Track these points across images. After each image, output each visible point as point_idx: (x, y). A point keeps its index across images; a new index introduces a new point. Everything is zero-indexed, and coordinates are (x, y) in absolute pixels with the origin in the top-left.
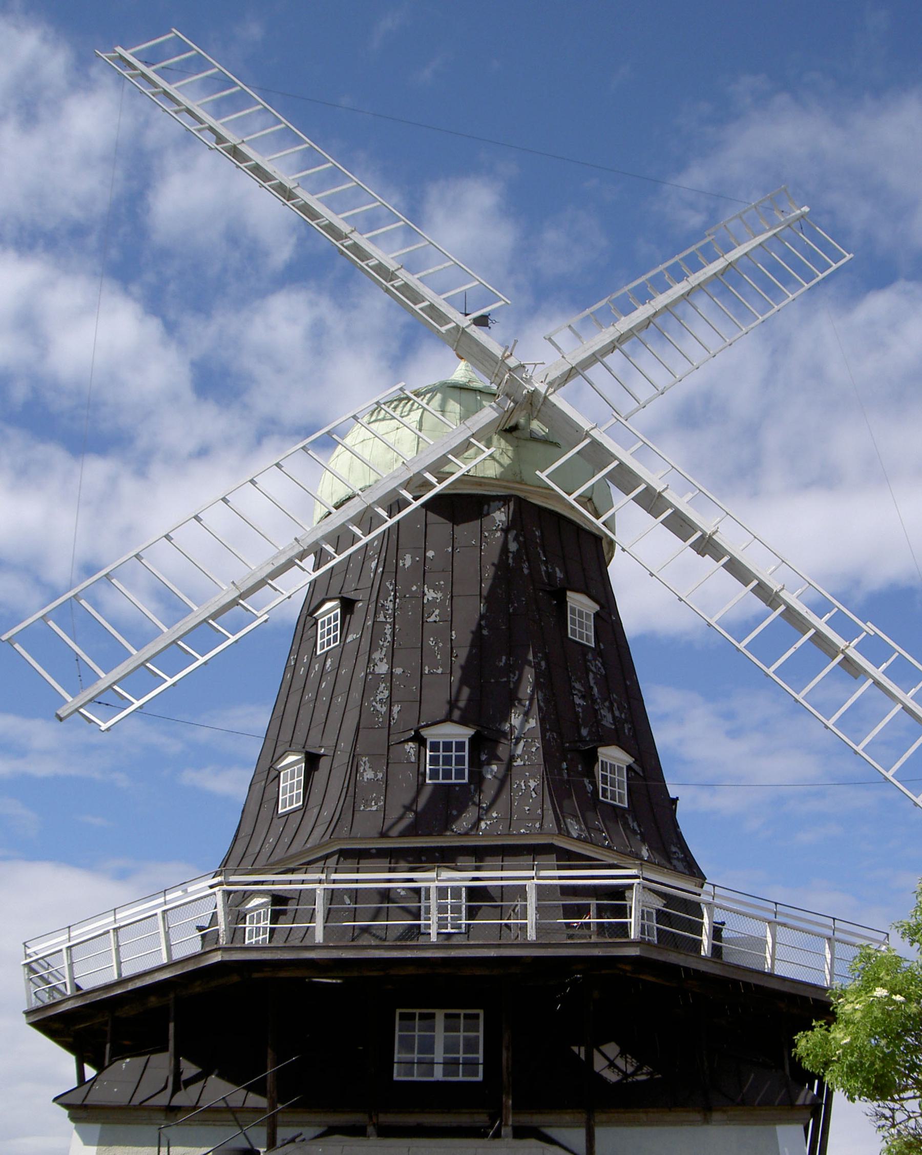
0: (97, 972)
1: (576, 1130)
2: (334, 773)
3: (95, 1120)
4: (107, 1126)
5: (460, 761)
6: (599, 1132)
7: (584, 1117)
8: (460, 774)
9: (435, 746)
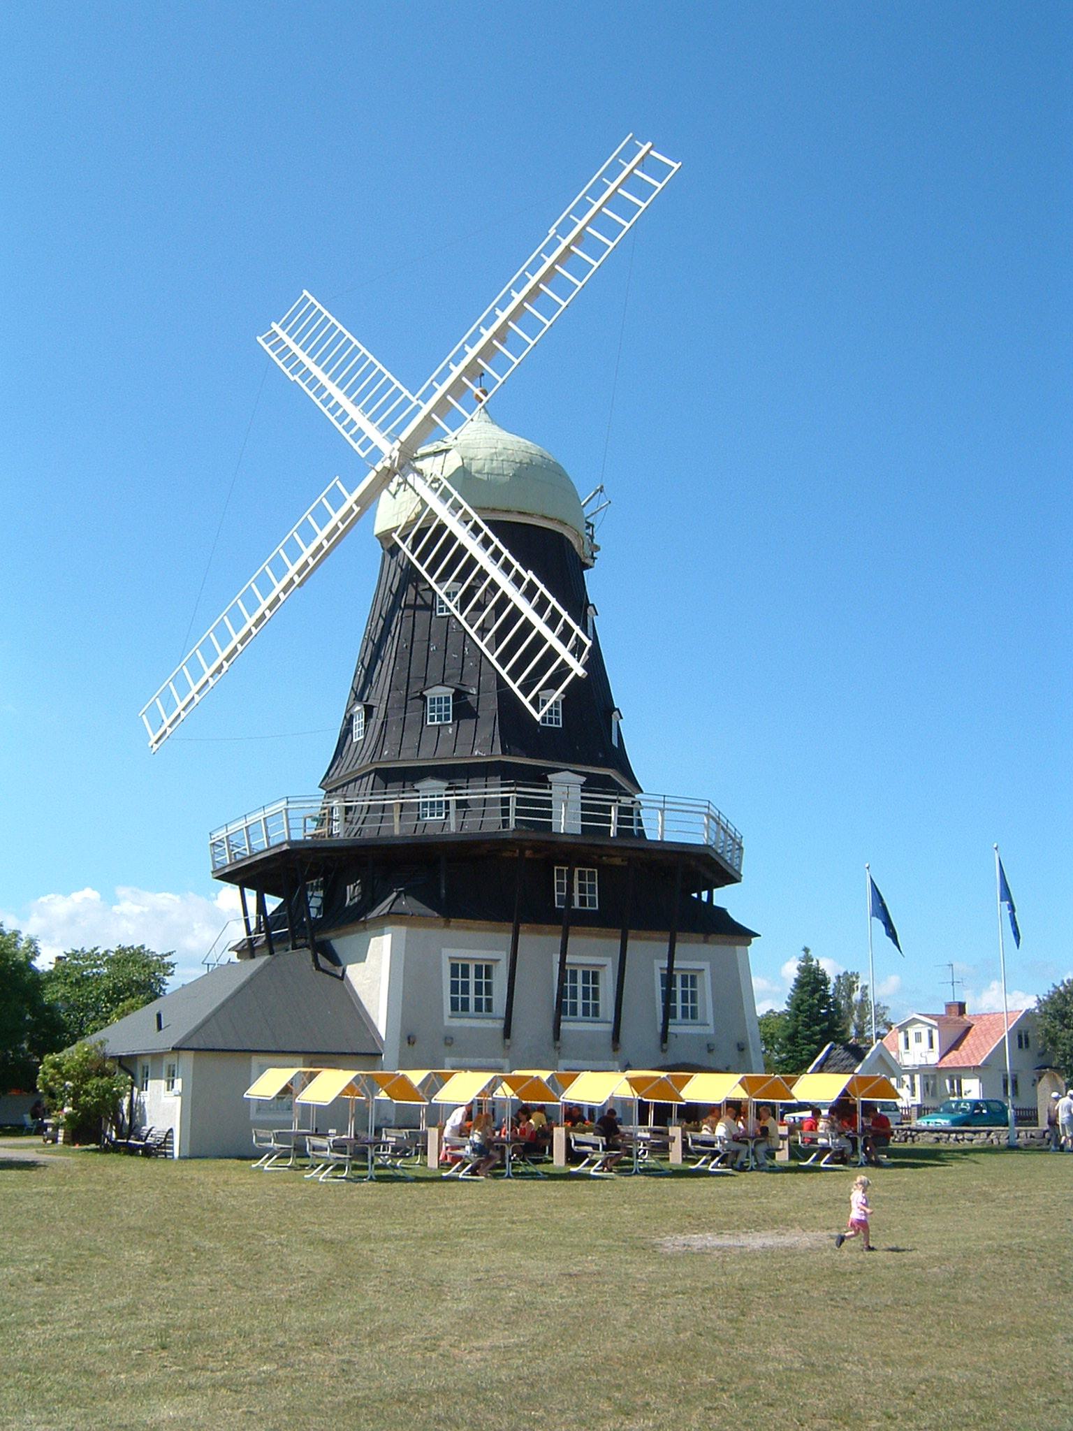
0: (261, 844)
1: (657, 944)
2: (377, 721)
3: (401, 923)
4: (414, 930)
5: (447, 709)
6: (630, 943)
7: (667, 935)
8: (557, 722)
9: (432, 702)
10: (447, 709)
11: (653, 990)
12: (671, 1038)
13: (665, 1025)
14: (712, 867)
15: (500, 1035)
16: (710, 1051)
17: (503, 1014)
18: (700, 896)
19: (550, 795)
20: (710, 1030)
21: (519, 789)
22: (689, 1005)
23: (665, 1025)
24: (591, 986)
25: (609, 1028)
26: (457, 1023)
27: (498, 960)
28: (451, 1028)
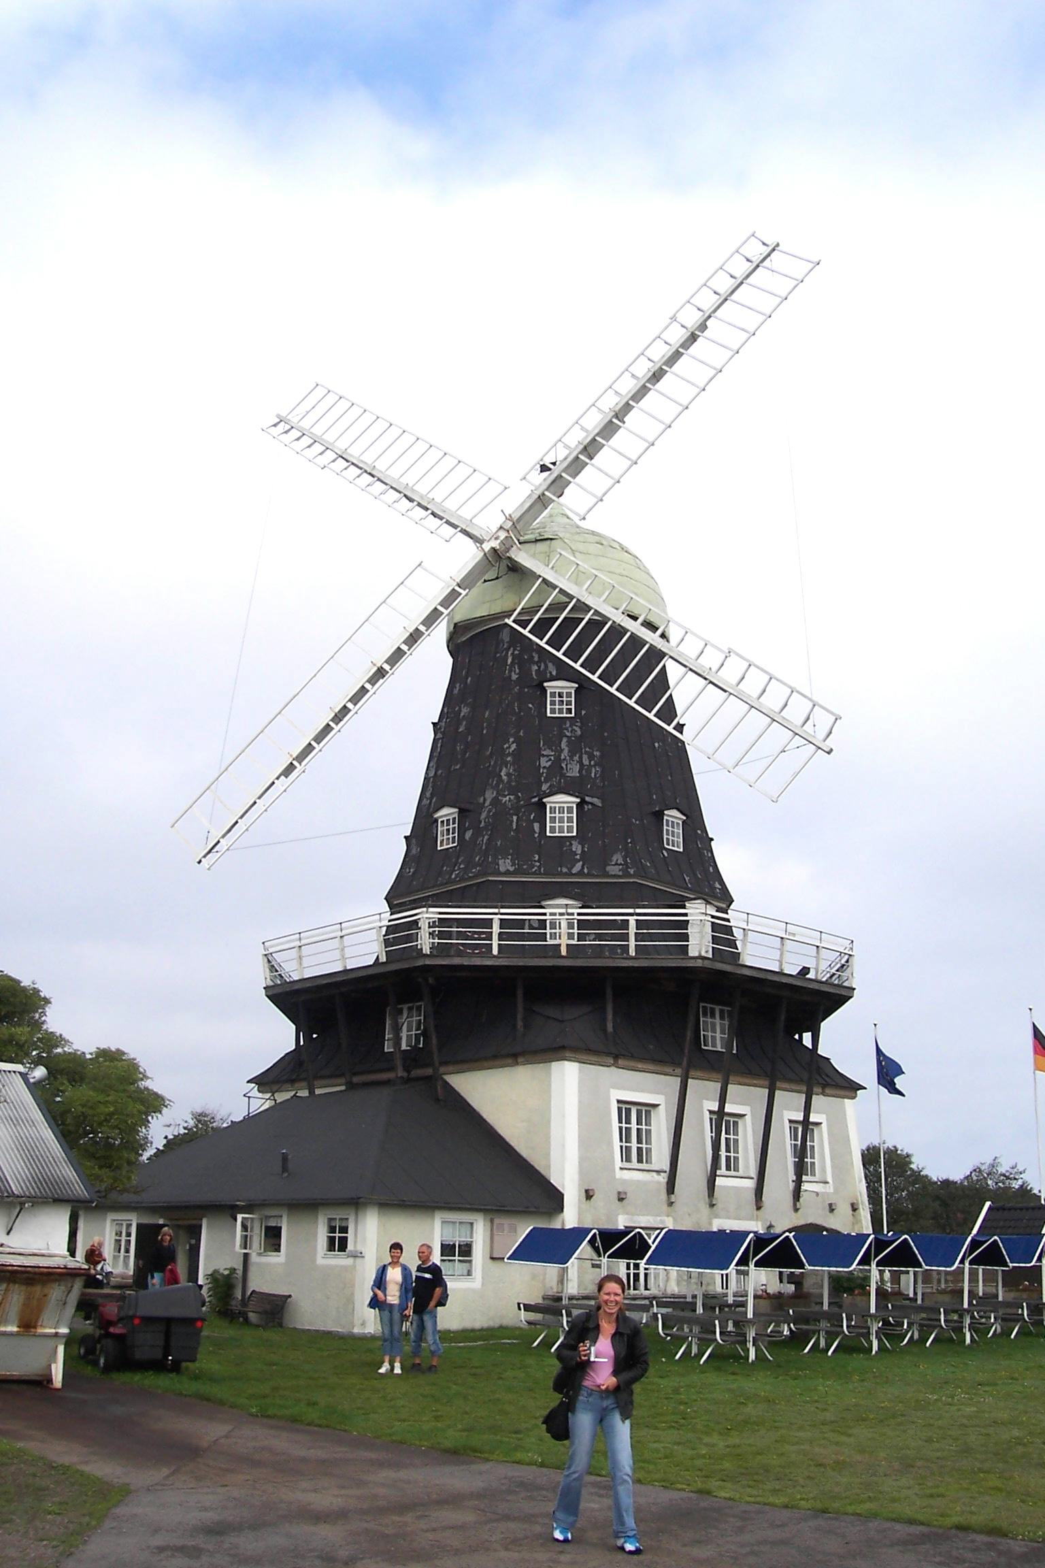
10: (553, 820)
11: (704, 1139)
12: (804, 1197)
13: (798, 1182)
14: (818, 999)
15: (664, 1191)
16: (832, 1210)
17: (667, 1167)
18: (801, 1037)
19: (686, 915)
20: (830, 1189)
21: (638, 911)
22: (644, 1146)
23: (798, 1182)
24: (644, 1127)
25: (750, 1184)
26: (627, 1175)
27: (658, 1105)
28: (624, 1182)
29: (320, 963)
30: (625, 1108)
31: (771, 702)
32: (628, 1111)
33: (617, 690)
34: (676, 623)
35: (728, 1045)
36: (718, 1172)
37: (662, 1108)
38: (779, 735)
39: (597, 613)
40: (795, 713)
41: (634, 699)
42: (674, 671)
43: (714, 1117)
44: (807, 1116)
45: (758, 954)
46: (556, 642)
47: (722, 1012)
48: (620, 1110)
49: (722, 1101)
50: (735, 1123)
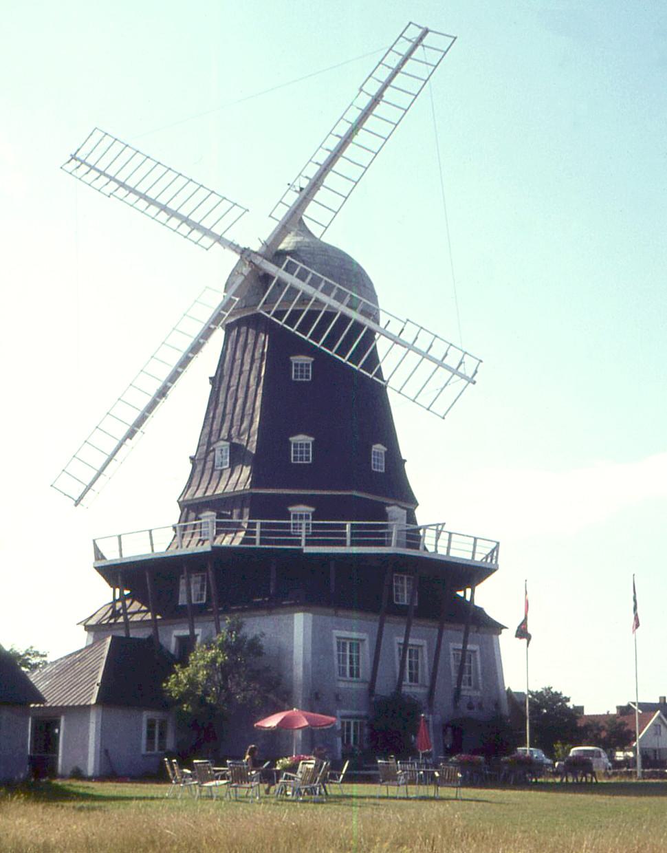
29: (137, 549)
30: (342, 644)
31: (437, 353)
32: (344, 644)
33: (336, 353)
34: (383, 311)
35: (412, 601)
36: (404, 683)
37: (367, 642)
38: (443, 374)
39: (329, 306)
40: (452, 361)
41: (334, 351)
42: (382, 344)
43: (402, 647)
44: (465, 647)
45: (432, 545)
46: (304, 328)
47: (408, 579)
48: (338, 643)
49: (465, 643)
50: (417, 652)
